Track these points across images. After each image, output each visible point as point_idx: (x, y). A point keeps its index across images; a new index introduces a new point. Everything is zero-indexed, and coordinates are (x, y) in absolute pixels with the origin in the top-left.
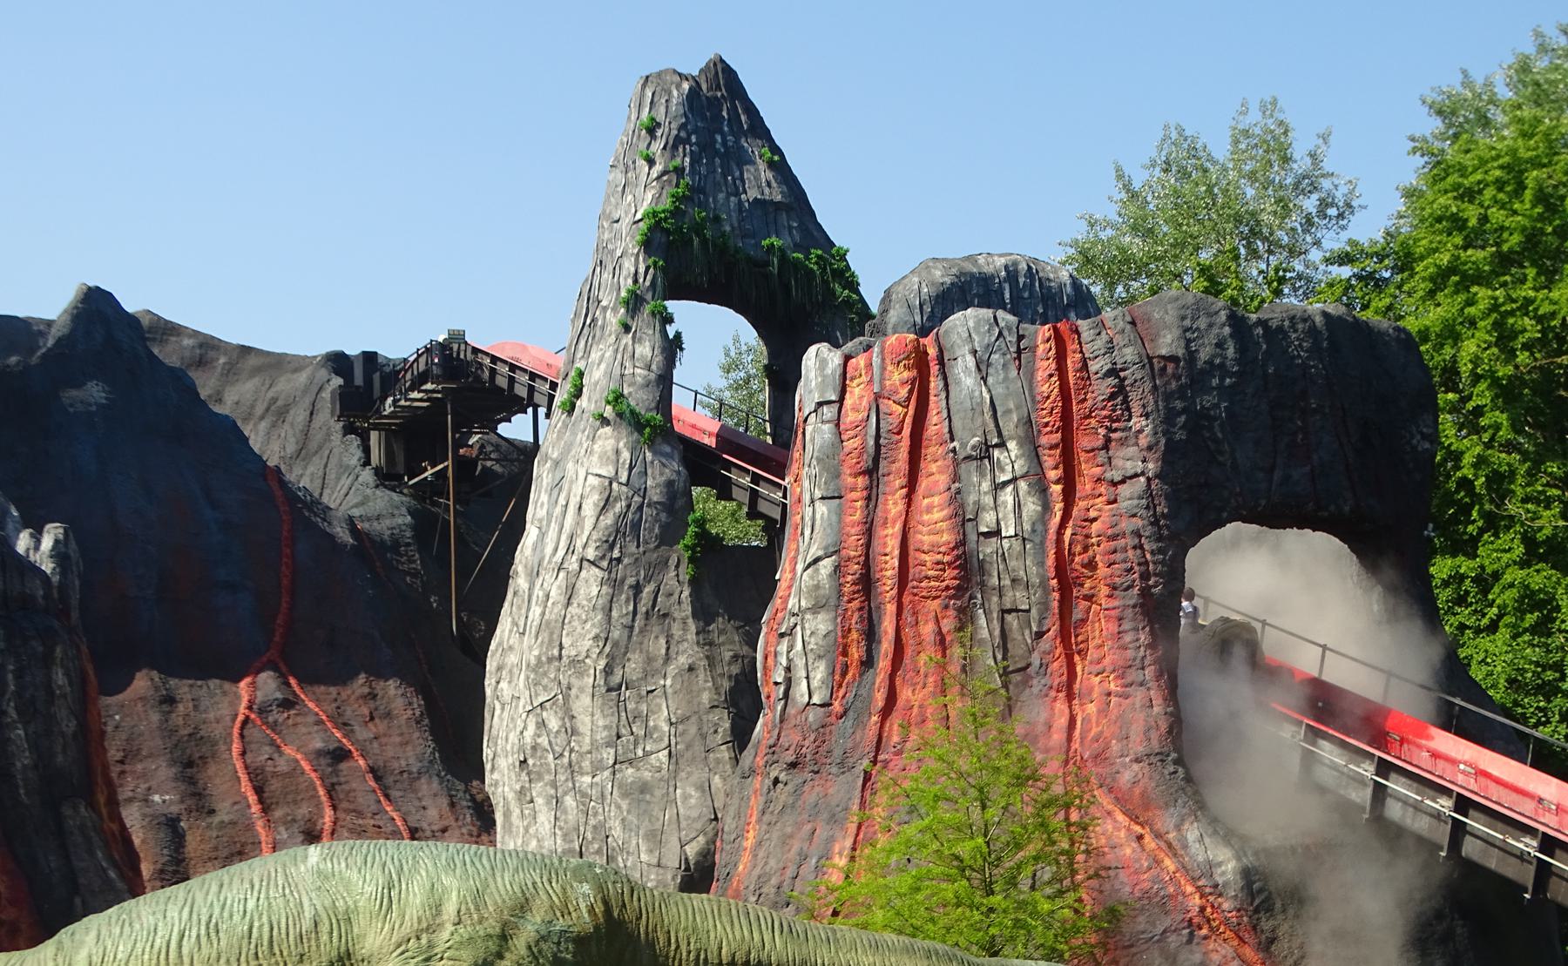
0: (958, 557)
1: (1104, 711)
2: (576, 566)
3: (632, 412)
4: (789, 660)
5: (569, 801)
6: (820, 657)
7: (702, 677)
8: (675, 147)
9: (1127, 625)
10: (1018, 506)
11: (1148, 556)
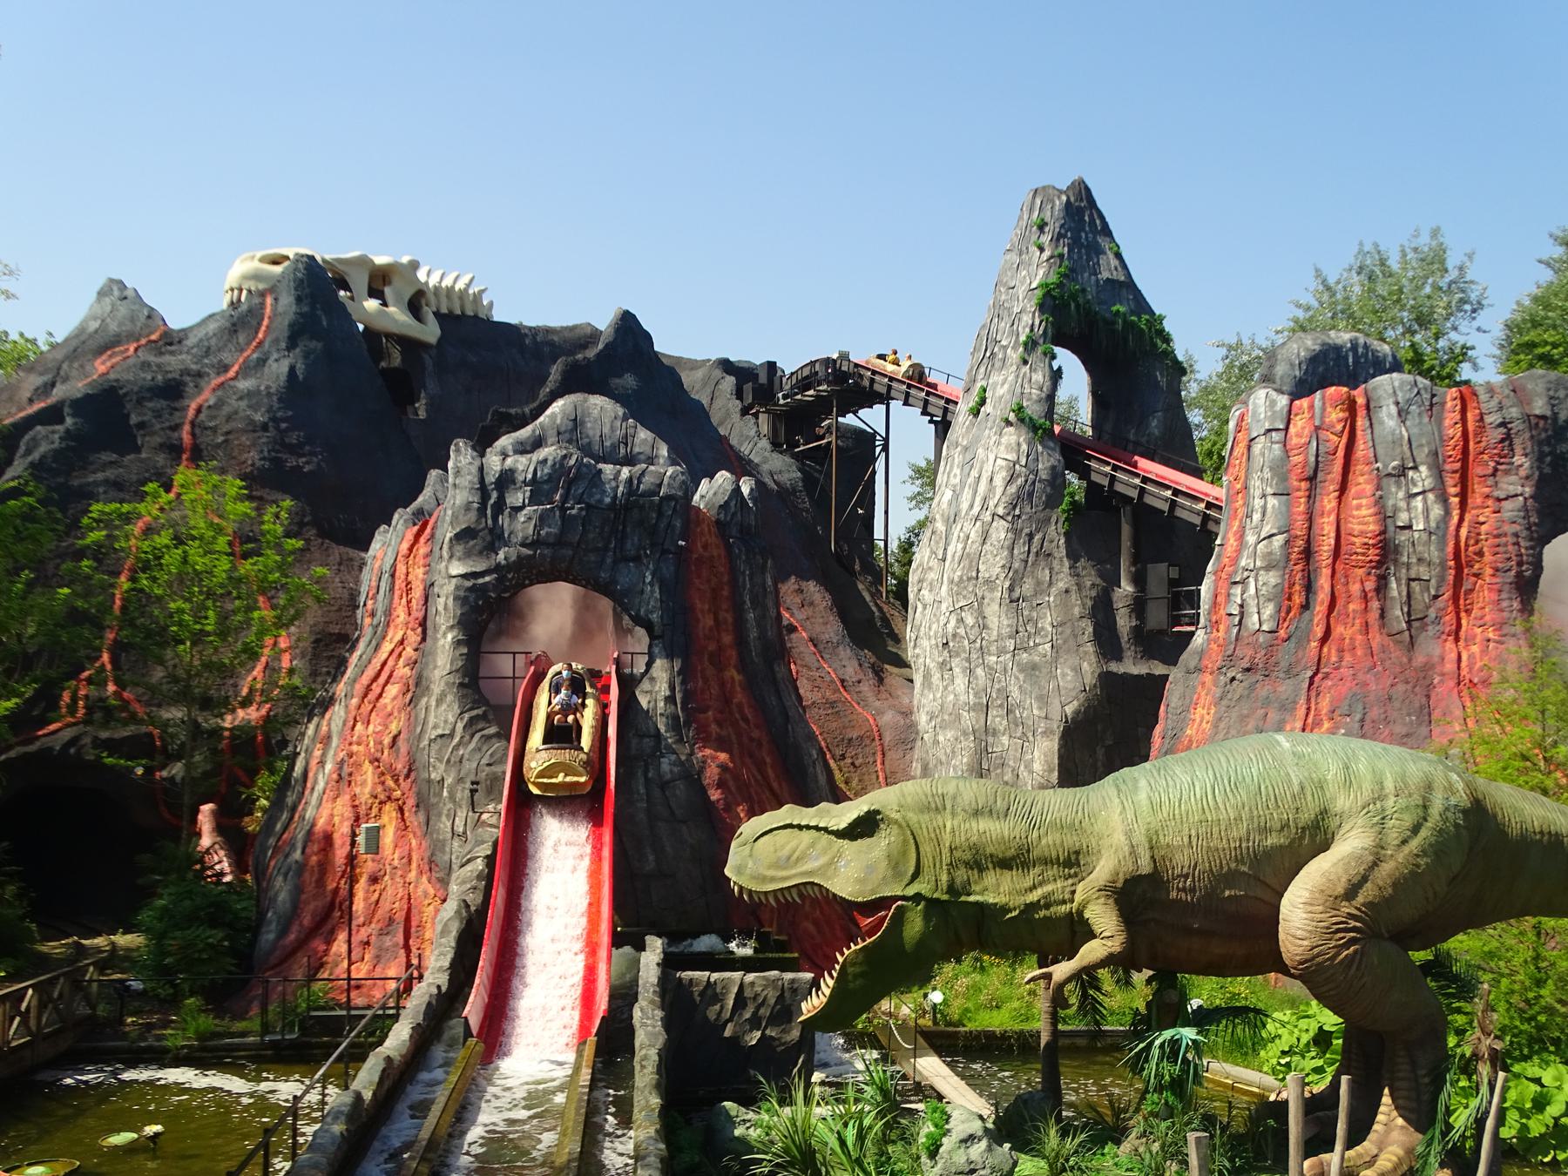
0: (1381, 541)
1: (1485, 651)
2: (989, 519)
3: (1031, 419)
4: (1243, 600)
5: (980, 672)
6: (1269, 600)
7: (1074, 597)
8: (1058, 240)
9: (1504, 595)
10: (1427, 511)
11: (1523, 550)
